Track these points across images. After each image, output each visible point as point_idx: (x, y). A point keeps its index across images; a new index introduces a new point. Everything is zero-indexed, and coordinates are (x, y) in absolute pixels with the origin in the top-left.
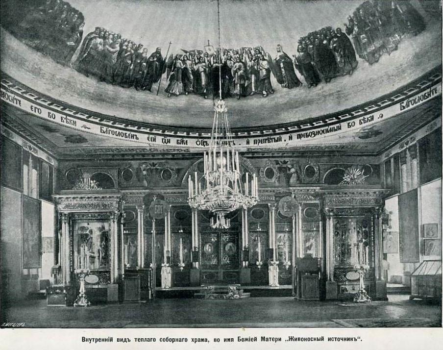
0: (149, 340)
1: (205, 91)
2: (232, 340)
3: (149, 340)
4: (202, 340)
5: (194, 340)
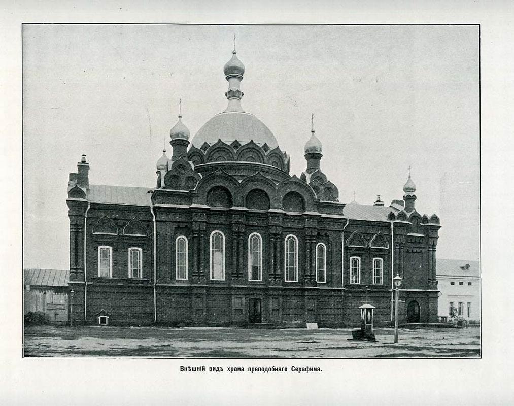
0: (280, 370)
1: (240, 181)
2: (243, 370)
3: (280, 370)
4: (315, 369)
5: (230, 369)
